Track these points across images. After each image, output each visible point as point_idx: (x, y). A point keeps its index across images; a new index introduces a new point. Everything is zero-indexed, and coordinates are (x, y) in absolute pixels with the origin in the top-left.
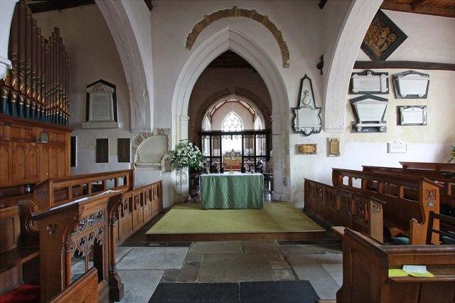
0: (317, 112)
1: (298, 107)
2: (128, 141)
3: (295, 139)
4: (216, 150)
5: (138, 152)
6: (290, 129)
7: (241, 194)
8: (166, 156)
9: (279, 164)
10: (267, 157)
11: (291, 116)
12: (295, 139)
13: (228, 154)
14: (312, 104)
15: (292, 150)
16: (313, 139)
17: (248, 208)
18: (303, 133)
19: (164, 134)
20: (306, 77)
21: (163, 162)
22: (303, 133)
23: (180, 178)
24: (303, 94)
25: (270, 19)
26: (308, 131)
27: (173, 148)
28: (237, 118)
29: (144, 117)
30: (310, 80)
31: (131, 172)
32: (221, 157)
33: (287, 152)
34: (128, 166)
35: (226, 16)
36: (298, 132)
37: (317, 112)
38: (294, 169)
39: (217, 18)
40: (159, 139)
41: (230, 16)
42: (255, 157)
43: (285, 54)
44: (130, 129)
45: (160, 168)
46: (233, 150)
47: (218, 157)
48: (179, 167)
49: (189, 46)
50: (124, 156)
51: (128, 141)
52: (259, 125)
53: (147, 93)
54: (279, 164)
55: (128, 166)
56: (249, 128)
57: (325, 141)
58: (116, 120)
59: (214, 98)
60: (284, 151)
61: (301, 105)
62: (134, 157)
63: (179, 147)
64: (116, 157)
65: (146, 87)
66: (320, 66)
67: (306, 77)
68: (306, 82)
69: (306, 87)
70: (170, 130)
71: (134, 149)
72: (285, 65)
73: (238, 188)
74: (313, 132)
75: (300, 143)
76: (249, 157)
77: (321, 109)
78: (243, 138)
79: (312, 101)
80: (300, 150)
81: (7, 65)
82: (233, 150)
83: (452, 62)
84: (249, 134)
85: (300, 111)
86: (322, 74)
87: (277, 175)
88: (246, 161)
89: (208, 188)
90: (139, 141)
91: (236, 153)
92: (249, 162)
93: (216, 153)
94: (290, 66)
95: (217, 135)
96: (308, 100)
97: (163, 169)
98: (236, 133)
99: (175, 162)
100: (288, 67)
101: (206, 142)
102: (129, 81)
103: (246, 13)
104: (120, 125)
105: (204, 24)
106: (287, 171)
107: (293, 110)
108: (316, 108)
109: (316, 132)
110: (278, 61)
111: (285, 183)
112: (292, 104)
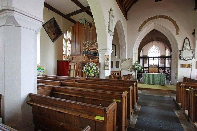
0: (191, 51)
1: (183, 50)
2: (119, 62)
3: (181, 62)
4: (146, 64)
5: (123, 65)
6: (179, 58)
7: (157, 80)
8: (131, 67)
9: (173, 71)
10: (170, 68)
11: (179, 53)
12: (181, 62)
13: (151, 66)
14: (189, 49)
15: (179, 66)
16: (189, 62)
17: (160, 85)
18: (185, 60)
19: (130, 60)
20: (187, 38)
21: (130, 69)
22: (185, 60)
23: (134, 74)
24: (185, 45)
25: (172, 18)
26: (187, 59)
27: (133, 64)
28: (156, 48)
29: (124, 54)
30: (189, 39)
31: (120, 71)
32: (148, 67)
33: (177, 67)
34: (119, 70)
35: (153, 19)
36: (182, 59)
37: (191, 51)
38: (180, 73)
39: (150, 20)
40: (128, 61)
41: (155, 19)
42: (165, 68)
43: (178, 30)
44: (120, 58)
45: (129, 70)
46: (154, 64)
47: (147, 67)
48: (135, 70)
49: (139, 30)
50: (117, 66)
51: (119, 62)
52: (167, 53)
53: (125, 47)
54: (173, 71)
55: (119, 70)
56: (163, 54)
57: (195, 63)
58: (115, 55)
59: (146, 42)
60: (176, 66)
61: (184, 49)
62: (120, 67)
63: (135, 64)
64: (115, 67)
65: (125, 46)
66: (194, 33)
67: (187, 38)
68: (187, 40)
69: (187, 41)
70: (132, 58)
71: (121, 64)
72: (177, 34)
73: (156, 78)
74: (189, 59)
75: (183, 63)
76: (162, 68)
77: (193, 50)
78: (159, 60)
79: (189, 47)
80: (183, 66)
81: (42, 22)
82: (154, 64)
83: (0, 130)
84: (163, 58)
85: (183, 51)
86: (194, 36)
87: (173, 75)
88: (159, 69)
89: (146, 77)
90: (122, 62)
91: (155, 66)
92: (162, 70)
93: (146, 65)
94: (179, 35)
95: (145, 58)
96: (187, 47)
97: (130, 71)
98: (171, 66)
99: (133, 69)
100: (179, 35)
101: (141, 61)
102: (120, 43)
103: (161, 17)
104: (117, 57)
105: (145, 23)
106: (177, 74)
107: (180, 51)
108: (191, 50)
109: (191, 59)
110: (174, 32)
111: (176, 78)
112: (180, 48)
